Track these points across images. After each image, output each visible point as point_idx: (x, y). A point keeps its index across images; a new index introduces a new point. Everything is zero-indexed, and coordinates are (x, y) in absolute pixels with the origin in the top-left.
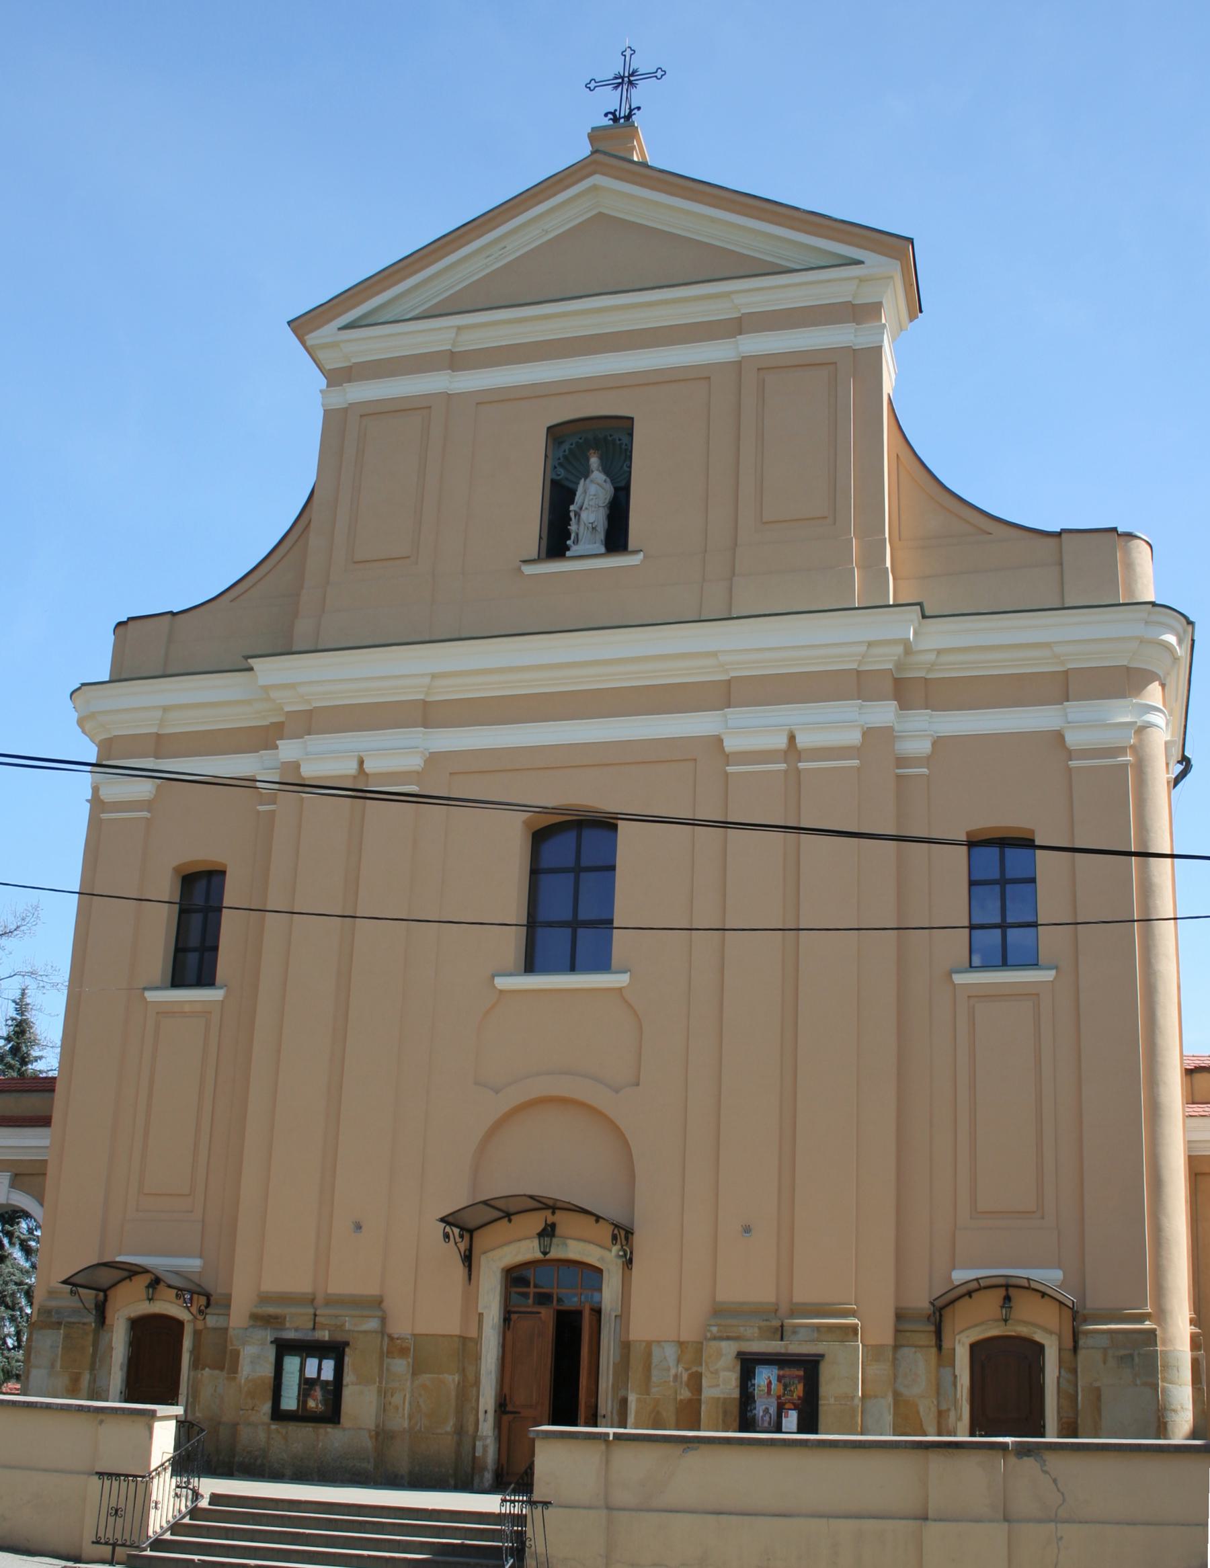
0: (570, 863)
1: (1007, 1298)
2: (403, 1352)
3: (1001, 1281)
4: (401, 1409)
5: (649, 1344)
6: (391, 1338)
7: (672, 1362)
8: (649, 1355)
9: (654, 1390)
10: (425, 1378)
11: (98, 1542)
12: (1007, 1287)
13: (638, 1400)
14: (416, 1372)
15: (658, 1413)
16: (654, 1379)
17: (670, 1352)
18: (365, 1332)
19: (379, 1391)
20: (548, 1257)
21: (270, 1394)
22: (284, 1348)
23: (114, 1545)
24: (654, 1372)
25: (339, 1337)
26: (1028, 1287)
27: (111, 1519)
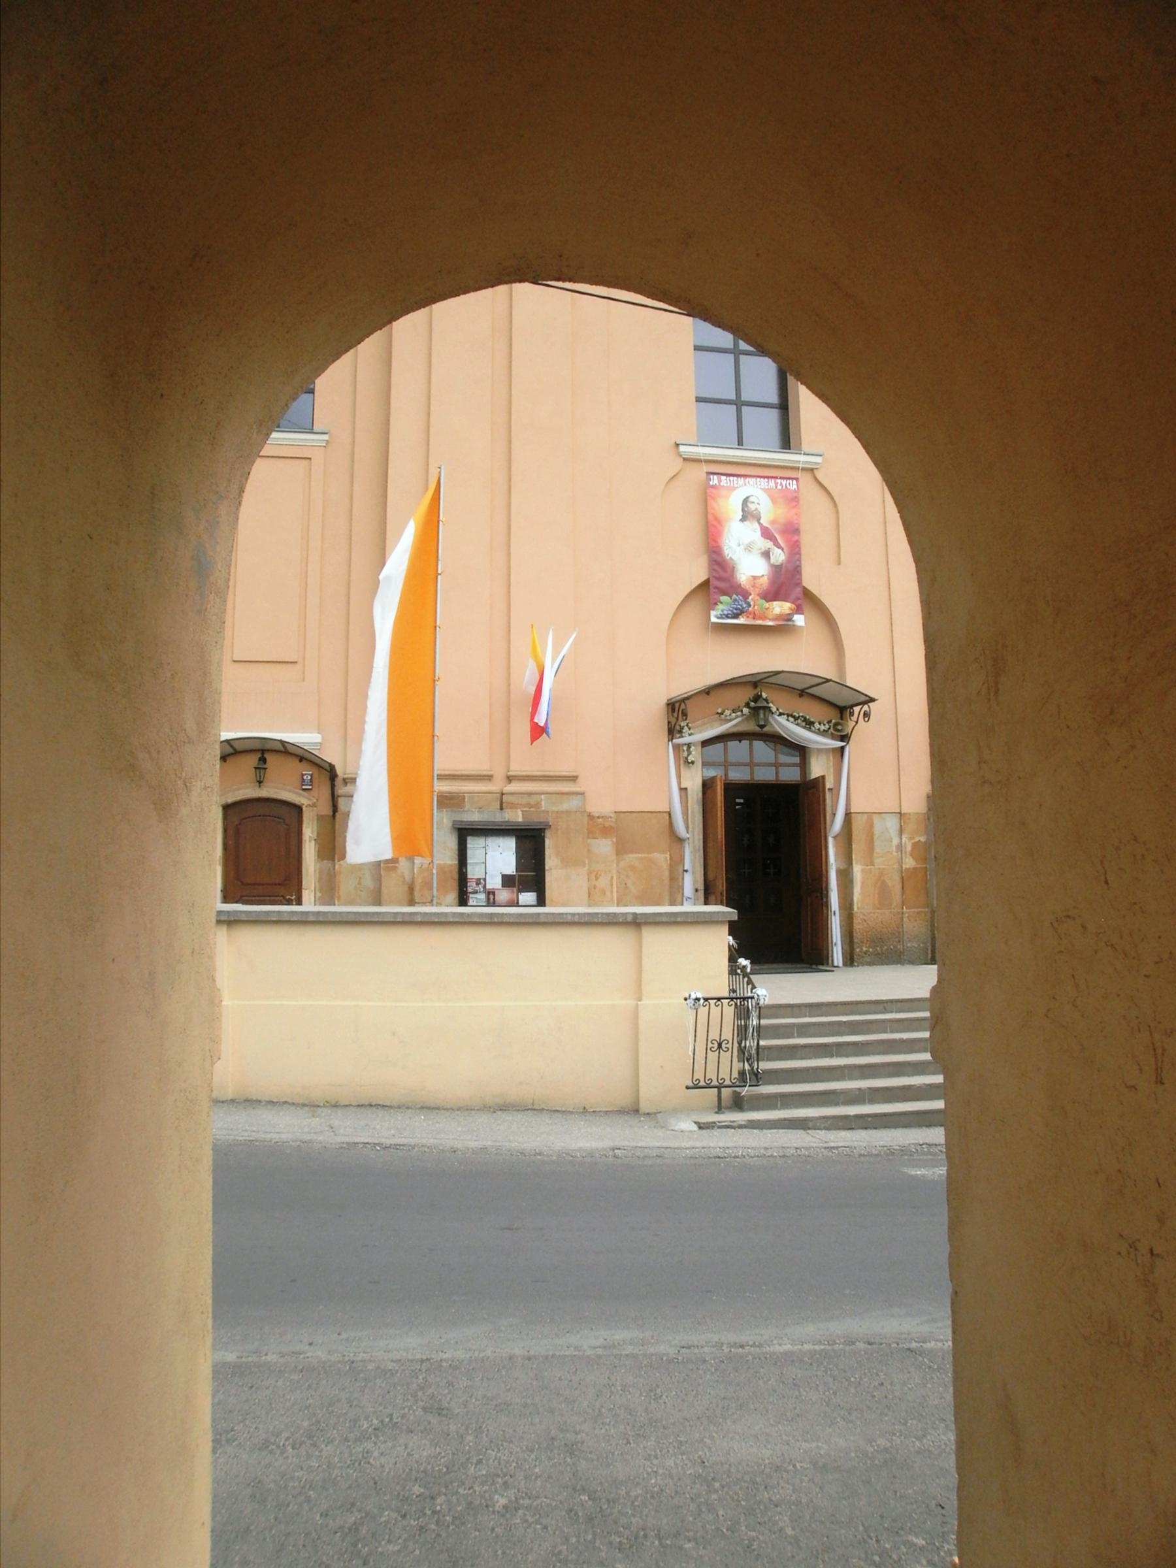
0: (744, 397)
1: (263, 760)
2: (606, 831)
3: (257, 746)
4: (608, 893)
5: (870, 814)
6: (591, 817)
7: (894, 833)
8: (871, 826)
9: (877, 861)
10: (632, 858)
11: (696, 1087)
12: (263, 751)
13: (863, 871)
14: (621, 850)
15: (884, 883)
16: (877, 850)
17: (892, 823)
18: (568, 812)
19: (589, 873)
20: (765, 729)
21: (455, 884)
22: (464, 833)
23: (719, 1088)
24: (877, 843)
25: (535, 819)
26: (285, 750)
27: (713, 1056)
